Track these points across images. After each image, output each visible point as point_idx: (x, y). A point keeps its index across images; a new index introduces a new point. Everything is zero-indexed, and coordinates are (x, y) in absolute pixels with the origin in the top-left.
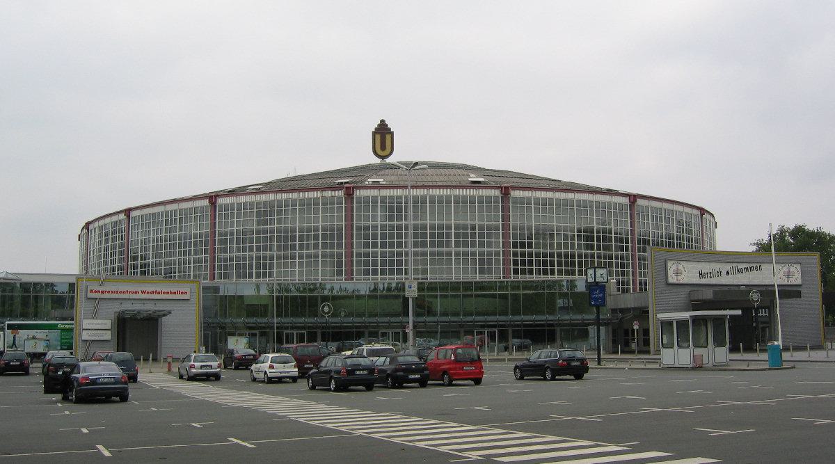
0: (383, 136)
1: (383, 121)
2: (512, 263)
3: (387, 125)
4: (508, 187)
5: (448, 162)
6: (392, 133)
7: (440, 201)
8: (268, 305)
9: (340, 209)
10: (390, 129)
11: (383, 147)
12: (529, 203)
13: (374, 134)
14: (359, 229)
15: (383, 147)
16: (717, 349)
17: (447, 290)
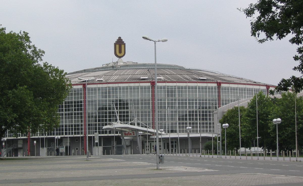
0: (120, 46)
1: (120, 38)
2: (8, 133)
3: (122, 40)
4: (220, 83)
5: (231, 74)
6: (125, 44)
7: (209, 89)
8: (241, 147)
9: (149, 92)
10: (123, 42)
11: (120, 52)
12: (228, 89)
13: (115, 44)
14: (89, 102)
15: (120, 52)
16: (272, 157)
17: (173, 145)
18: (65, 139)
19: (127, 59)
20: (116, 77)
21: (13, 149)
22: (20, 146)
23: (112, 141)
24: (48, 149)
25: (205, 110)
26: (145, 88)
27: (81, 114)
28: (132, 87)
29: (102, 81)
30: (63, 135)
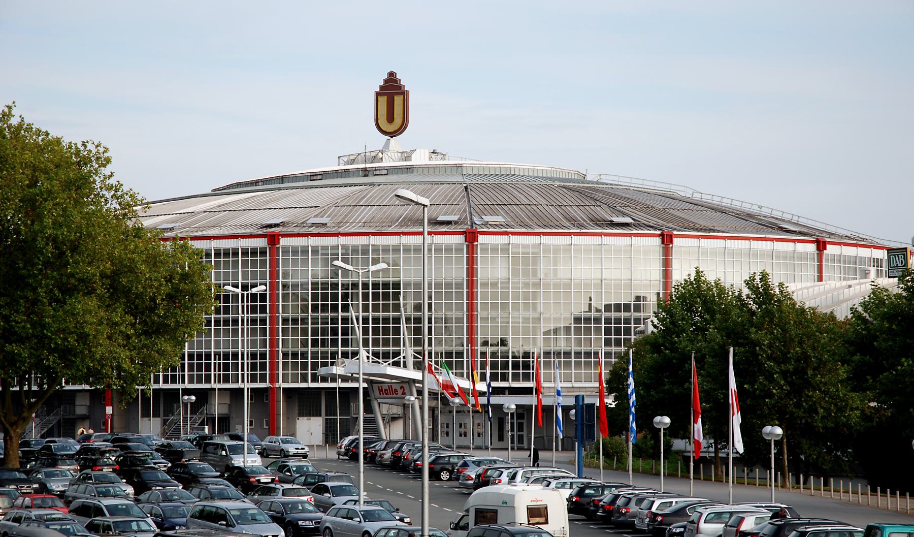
11: (390, 118)
13: (378, 95)
15: (390, 118)
18: (78, 394)
19: (416, 145)
20: (367, 213)
21: (59, 422)
22: (81, 410)
23: (175, 405)
24: (165, 422)
25: (623, 315)
26: (449, 249)
27: (263, 321)
28: (488, 245)
29: (324, 225)
30: (508, 381)
